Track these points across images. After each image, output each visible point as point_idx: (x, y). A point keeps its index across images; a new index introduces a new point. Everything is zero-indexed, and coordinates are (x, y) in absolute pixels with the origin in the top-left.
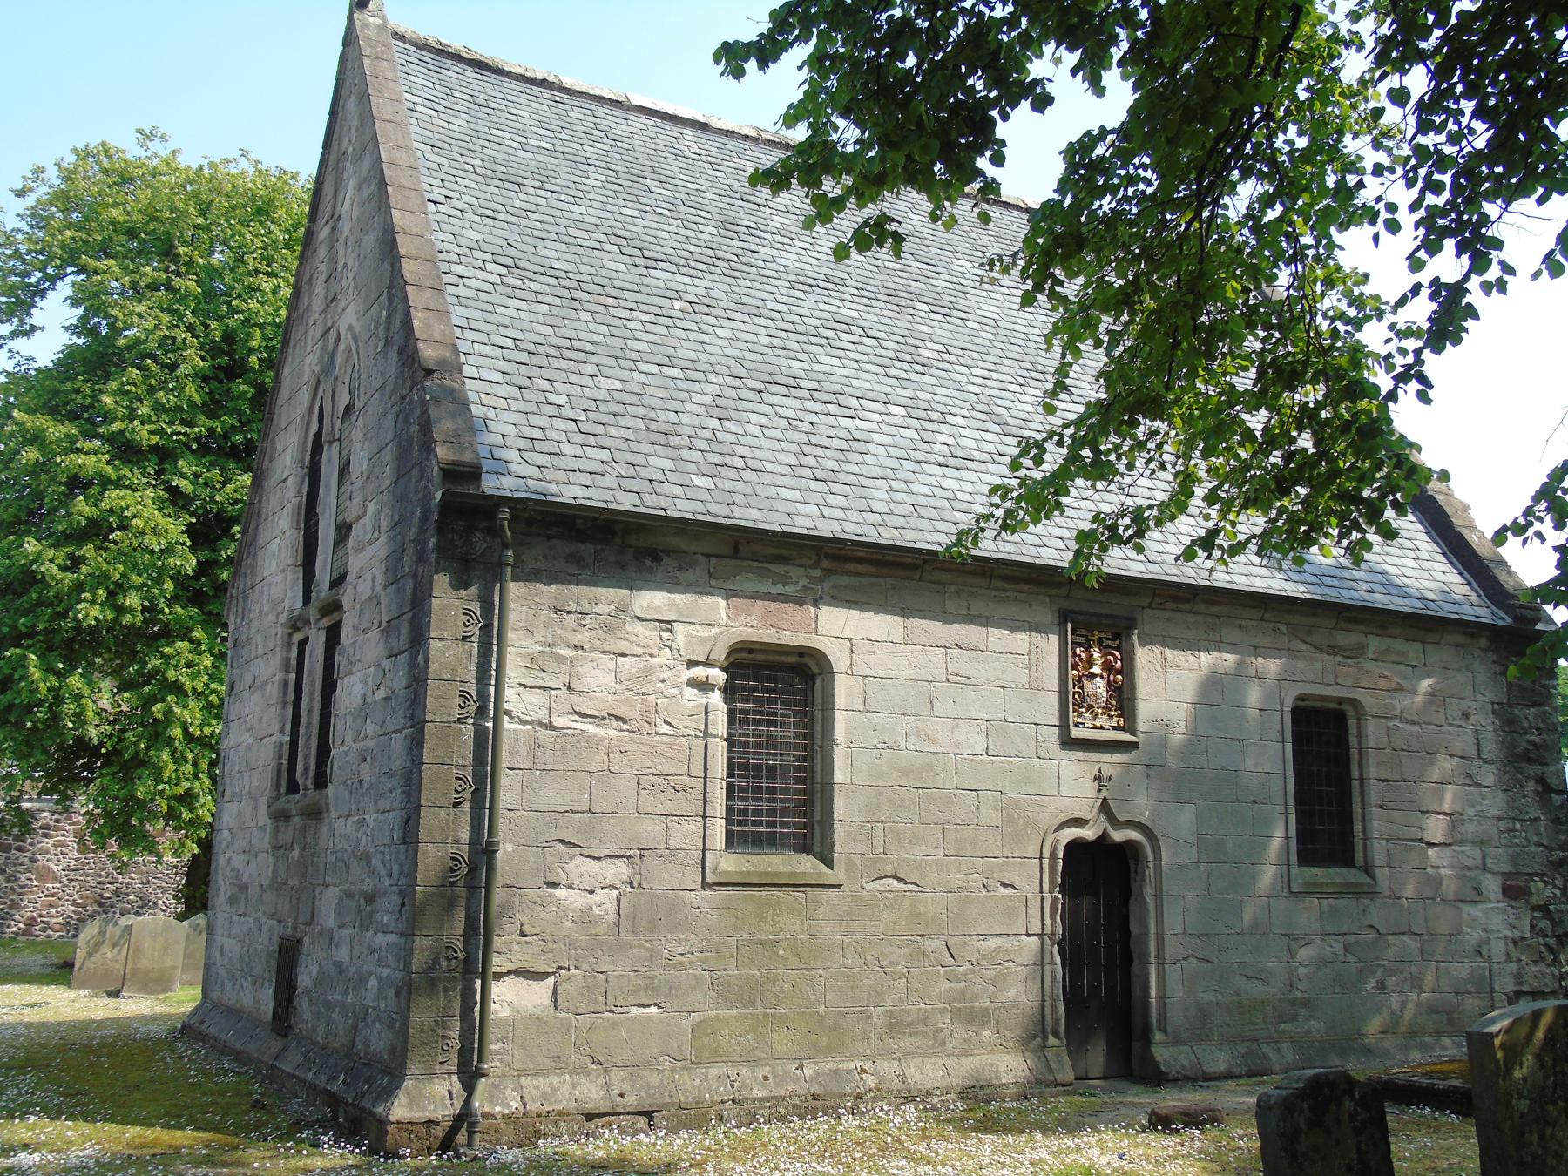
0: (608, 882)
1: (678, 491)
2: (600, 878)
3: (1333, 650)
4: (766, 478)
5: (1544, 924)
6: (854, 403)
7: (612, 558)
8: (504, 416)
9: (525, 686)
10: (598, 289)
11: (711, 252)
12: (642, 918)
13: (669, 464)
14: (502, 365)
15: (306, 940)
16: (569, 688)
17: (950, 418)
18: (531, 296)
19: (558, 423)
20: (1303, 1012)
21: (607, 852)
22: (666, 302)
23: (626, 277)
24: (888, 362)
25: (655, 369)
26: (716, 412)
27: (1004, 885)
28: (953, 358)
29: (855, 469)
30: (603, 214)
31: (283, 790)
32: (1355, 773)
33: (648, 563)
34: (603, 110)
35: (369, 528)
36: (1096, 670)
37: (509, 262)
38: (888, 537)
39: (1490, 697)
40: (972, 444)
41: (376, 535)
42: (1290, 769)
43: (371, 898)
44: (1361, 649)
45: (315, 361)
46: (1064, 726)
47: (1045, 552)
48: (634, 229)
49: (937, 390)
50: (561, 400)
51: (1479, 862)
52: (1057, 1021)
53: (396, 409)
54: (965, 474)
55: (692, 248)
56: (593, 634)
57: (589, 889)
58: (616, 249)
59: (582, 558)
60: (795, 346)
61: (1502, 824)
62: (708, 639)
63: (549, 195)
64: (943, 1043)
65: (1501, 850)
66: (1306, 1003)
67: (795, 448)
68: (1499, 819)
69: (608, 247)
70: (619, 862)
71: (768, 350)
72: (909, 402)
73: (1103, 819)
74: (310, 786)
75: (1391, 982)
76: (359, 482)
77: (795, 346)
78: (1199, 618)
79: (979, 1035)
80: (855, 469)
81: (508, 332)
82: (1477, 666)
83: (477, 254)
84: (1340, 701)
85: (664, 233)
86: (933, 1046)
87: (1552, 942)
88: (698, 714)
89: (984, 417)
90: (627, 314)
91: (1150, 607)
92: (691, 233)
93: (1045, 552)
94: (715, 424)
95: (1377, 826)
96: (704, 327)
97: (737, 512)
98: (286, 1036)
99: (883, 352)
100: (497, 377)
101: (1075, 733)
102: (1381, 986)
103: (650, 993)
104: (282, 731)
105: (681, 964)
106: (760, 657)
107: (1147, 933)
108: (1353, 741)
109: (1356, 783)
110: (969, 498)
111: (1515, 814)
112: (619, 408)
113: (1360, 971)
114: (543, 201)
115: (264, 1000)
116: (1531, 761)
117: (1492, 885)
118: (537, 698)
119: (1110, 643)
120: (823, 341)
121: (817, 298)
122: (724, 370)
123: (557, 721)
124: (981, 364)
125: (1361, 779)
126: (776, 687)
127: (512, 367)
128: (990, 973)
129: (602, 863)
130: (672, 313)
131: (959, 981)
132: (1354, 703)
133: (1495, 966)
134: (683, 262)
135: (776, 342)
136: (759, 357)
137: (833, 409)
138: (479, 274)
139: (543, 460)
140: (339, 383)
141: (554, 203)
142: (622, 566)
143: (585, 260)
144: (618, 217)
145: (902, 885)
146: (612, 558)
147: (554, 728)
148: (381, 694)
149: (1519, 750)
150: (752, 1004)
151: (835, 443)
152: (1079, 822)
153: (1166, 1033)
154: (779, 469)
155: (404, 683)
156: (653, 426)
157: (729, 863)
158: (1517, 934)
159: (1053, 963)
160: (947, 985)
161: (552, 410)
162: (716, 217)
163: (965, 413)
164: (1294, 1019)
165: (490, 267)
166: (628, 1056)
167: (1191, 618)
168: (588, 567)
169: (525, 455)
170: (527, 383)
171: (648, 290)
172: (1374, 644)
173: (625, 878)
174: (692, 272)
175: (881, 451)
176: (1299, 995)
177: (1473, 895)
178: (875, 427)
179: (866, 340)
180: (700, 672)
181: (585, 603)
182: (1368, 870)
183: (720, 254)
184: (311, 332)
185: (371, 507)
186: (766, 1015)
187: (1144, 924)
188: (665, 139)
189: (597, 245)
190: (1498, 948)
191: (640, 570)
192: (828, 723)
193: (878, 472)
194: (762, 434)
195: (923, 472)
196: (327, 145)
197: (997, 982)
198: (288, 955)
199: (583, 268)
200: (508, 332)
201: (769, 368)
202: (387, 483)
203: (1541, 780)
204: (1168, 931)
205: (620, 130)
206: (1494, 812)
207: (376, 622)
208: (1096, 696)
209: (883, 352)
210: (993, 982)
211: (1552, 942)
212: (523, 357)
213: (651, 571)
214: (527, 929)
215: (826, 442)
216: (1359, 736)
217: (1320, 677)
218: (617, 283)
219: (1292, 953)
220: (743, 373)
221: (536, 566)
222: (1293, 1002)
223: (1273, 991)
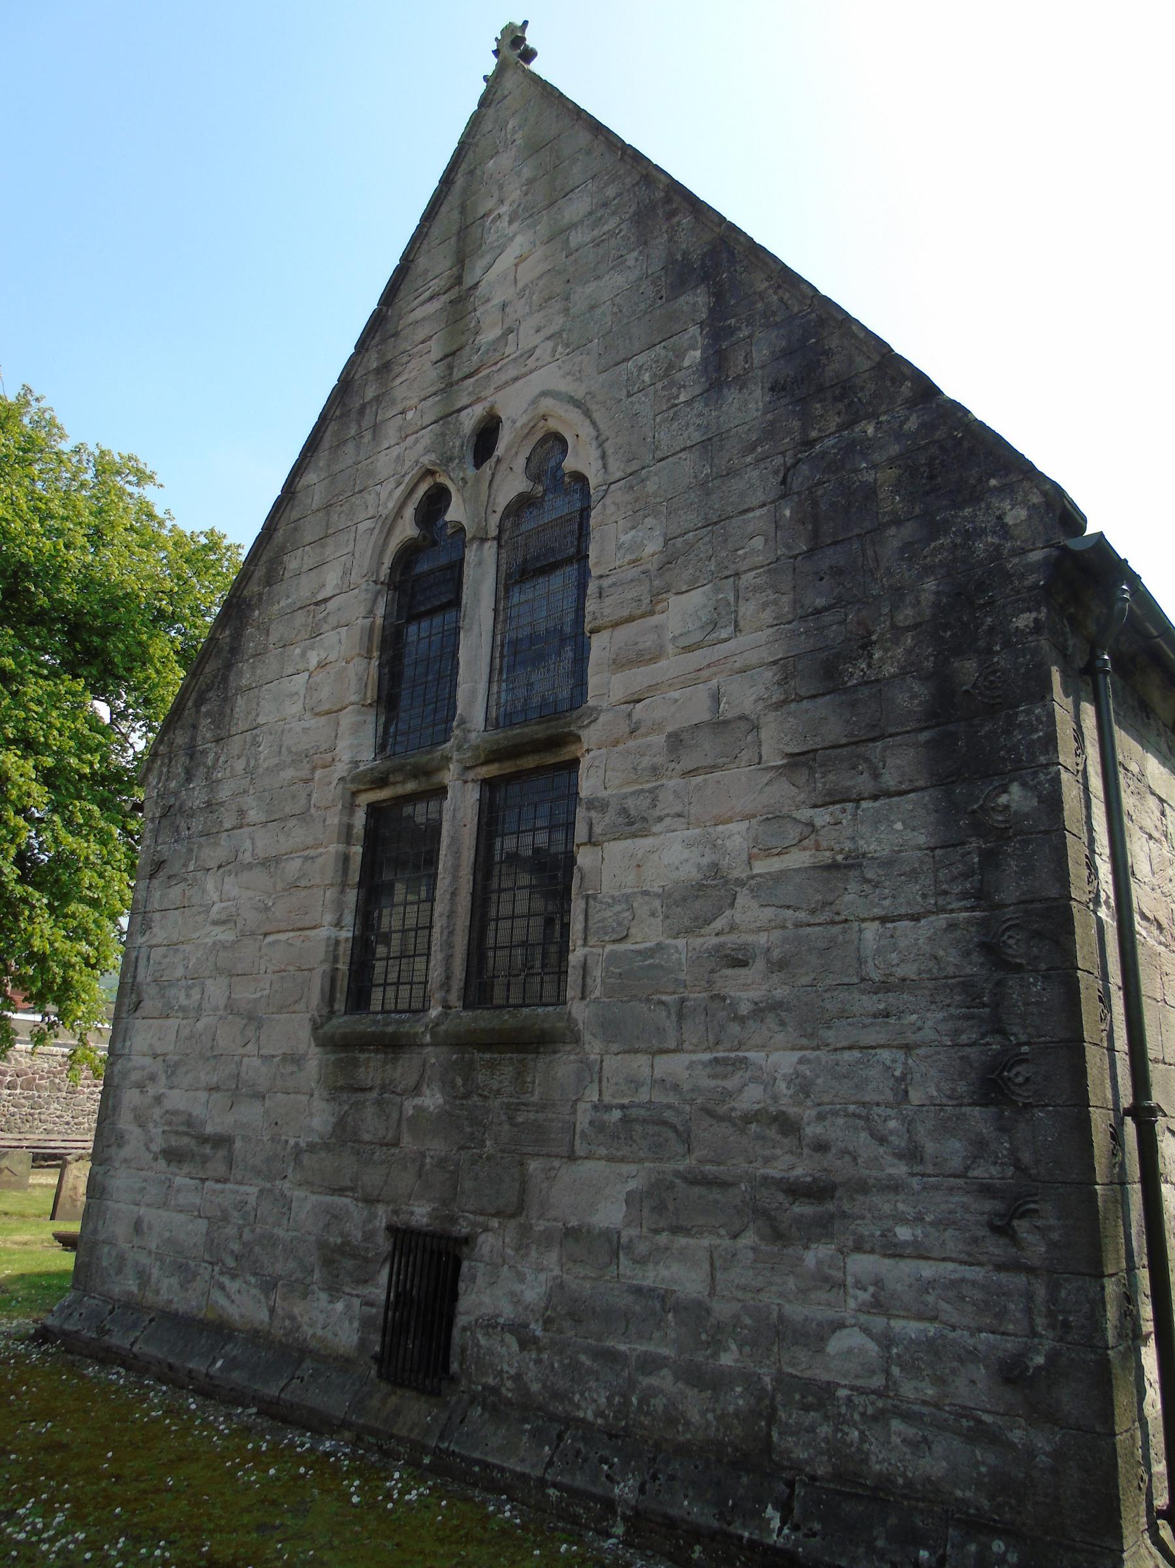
15: (487, 1243)
31: (340, 1006)
74: (454, 998)
104: (338, 924)
198: (429, 1270)
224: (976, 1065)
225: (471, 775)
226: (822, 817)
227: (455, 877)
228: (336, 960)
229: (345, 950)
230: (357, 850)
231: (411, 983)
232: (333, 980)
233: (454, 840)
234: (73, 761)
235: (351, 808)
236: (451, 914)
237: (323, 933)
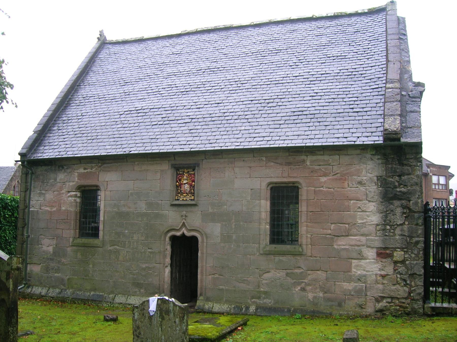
7: (53, 169)
12: (59, 252)
27: (149, 248)
33: (61, 168)
39: (376, 174)
44: (304, 161)
61: (378, 228)
65: (378, 238)
66: (265, 293)
68: (377, 225)
78: (226, 160)
84: (294, 183)
126: (89, 195)
131: (134, 275)
132: (298, 182)
133: (368, 285)
164: (259, 298)
167: (222, 160)
176: (262, 289)
192: (271, 194)
198: (27, 334)
213: (61, 170)
217: (278, 174)
222: (260, 292)
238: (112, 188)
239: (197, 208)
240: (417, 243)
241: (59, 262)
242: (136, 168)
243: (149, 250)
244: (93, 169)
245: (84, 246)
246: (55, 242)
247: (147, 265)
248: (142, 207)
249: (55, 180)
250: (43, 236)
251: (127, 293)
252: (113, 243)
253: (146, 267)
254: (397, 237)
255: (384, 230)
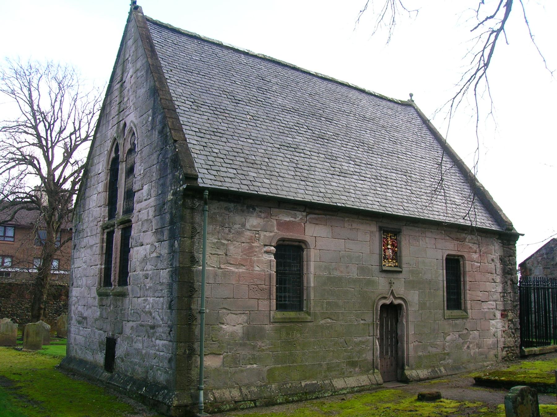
0: (239, 322)
1: (259, 184)
2: (237, 321)
3: (457, 239)
4: (286, 180)
5: (512, 326)
6: (309, 153)
8: (200, 157)
9: (211, 254)
10: (222, 111)
11: (255, 98)
12: (252, 334)
13: (255, 175)
14: (196, 138)
15: (119, 340)
16: (226, 255)
17: (339, 159)
18: (201, 113)
19: (218, 160)
20: (447, 357)
21: (239, 312)
22: (244, 116)
23: (231, 107)
24: (316, 139)
25: (245, 140)
26: (266, 156)
27: (362, 320)
28: (335, 138)
29: (313, 177)
30: (220, 84)
31: (102, 285)
32: (462, 279)
33: (251, 210)
34: (214, 47)
35: (145, 194)
36: (389, 247)
37: (193, 100)
38: (327, 202)
40: (346, 168)
41: (149, 197)
42: (445, 279)
43: (153, 327)
44: (465, 239)
45: (114, 132)
46: (381, 265)
47: (374, 207)
48: (230, 89)
49: (333, 149)
50: (217, 151)
51: (495, 307)
52: (378, 364)
53: (158, 153)
54: (347, 179)
55: (249, 96)
56: (233, 235)
57: (233, 326)
58: (226, 96)
59: (230, 208)
60: (287, 132)
61: (501, 294)
62: (270, 236)
63: (201, 76)
64: (344, 373)
66: (448, 354)
67: (293, 169)
68: (500, 293)
69: (223, 95)
70: (243, 316)
71: (279, 133)
72: (325, 153)
73: (391, 297)
74: (116, 284)
75: (471, 346)
76: (139, 178)
77: (287, 132)
78: (420, 229)
79: (355, 370)
80: (313, 177)
81: (196, 126)
82: (495, 244)
83: (182, 98)
84: (458, 256)
85: (241, 93)
86: (340, 374)
87: (513, 331)
88: (265, 262)
89: (348, 159)
90: (232, 120)
91: (405, 225)
92: (248, 91)
93: (374, 207)
94: (267, 160)
95: (470, 295)
96: (258, 125)
97: (280, 192)
98: (112, 372)
99: (314, 135)
100: (195, 142)
101: (384, 268)
102: (468, 347)
103: (254, 360)
104: (101, 264)
105: (263, 350)
106: (287, 243)
107: (404, 334)
108: (462, 269)
109: (462, 283)
110: (348, 187)
111: (504, 291)
112: (236, 154)
113: (463, 343)
114: (200, 79)
115: (100, 358)
116: (509, 274)
117: (498, 314)
118: (215, 258)
119: (393, 238)
120: (295, 131)
121: (291, 115)
122: (267, 141)
123: (222, 266)
124: (345, 140)
125: (464, 281)
126: (290, 254)
127: (199, 139)
128: (357, 349)
129: (238, 316)
130: (247, 120)
132: (462, 257)
134: (247, 101)
135: (281, 131)
136: (277, 136)
137: (302, 155)
138: (184, 105)
139: (215, 173)
140: (126, 141)
141: (204, 80)
142: (243, 211)
143: (216, 100)
144: (225, 85)
145: (332, 321)
146: (240, 208)
147: (222, 269)
148: (154, 255)
149: (506, 271)
150: (285, 362)
151: (305, 167)
152: (385, 298)
153: (409, 366)
154: (289, 177)
155: (166, 251)
156: (248, 161)
157: (279, 315)
158: (504, 329)
159: (376, 345)
160: (345, 354)
161: (215, 155)
162: (256, 86)
163: (343, 157)
164: (444, 359)
165: (187, 102)
166: (247, 382)
167: (417, 229)
168: (231, 211)
169: (209, 171)
170: (205, 145)
171: (238, 111)
172: (469, 237)
173: (245, 320)
174: (252, 105)
175: (320, 170)
176: (446, 351)
177: (493, 318)
178: (316, 162)
179: (308, 131)
180: (266, 248)
181: (231, 224)
182: (465, 310)
183: (259, 99)
184: (111, 122)
185: (146, 187)
186: (290, 366)
187: (402, 331)
188: (235, 58)
189: (219, 95)
190: (499, 334)
191: (248, 212)
193: (320, 178)
194: (281, 164)
195: (333, 178)
196: (119, 56)
197: (360, 352)
198: (110, 345)
199: (217, 103)
200: (196, 126)
201: (280, 140)
202: (154, 179)
203: (512, 280)
204: (410, 333)
205: (220, 54)
206: (500, 291)
207: (150, 229)
208: (390, 256)
209: (314, 135)
210: (359, 352)
211: (513, 331)
212: (202, 135)
213: (252, 213)
214: (214, 339)
215: (302, 167)
216: (464, 267)
218: (228, 109)
219: (445, 339)
220: (273, 142)
221: (215, 211)
223: (439, 350)
224: (478, 276)
225: (119, 227)
226: (157, 244)
227: (116, 254)
228: (101, 273)
229: (103, 271)
230: (105, 244)
231: (446, 207)
232: (101, 278)
233: (116, 244)
234: (168, 130)
235: (103, 234)
236: (116, 263)
237: (99, 266)
238: (322, 244)
239: (401, 274)
240: (517, 305)
241: (254, 347)
242: (346, 225)
243: (362, 322)
244: (298, 219)
245: (291, 321)
246: (244, 318)
247: (360, 339)
248: (354, 273)
249: (243, 225)
250: (225, 311)
251: (342, 375)
252: (325, 316)
253: (360, 341)
254: (509, 302)
255: (503, 296)
